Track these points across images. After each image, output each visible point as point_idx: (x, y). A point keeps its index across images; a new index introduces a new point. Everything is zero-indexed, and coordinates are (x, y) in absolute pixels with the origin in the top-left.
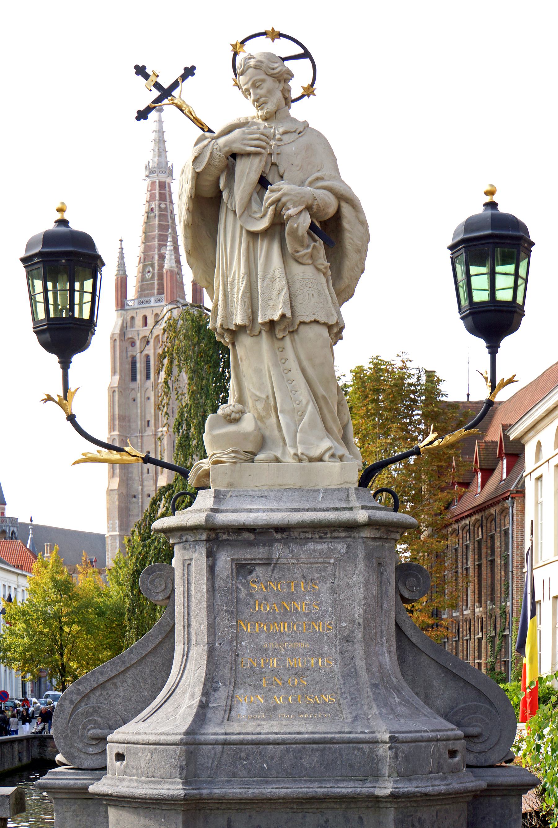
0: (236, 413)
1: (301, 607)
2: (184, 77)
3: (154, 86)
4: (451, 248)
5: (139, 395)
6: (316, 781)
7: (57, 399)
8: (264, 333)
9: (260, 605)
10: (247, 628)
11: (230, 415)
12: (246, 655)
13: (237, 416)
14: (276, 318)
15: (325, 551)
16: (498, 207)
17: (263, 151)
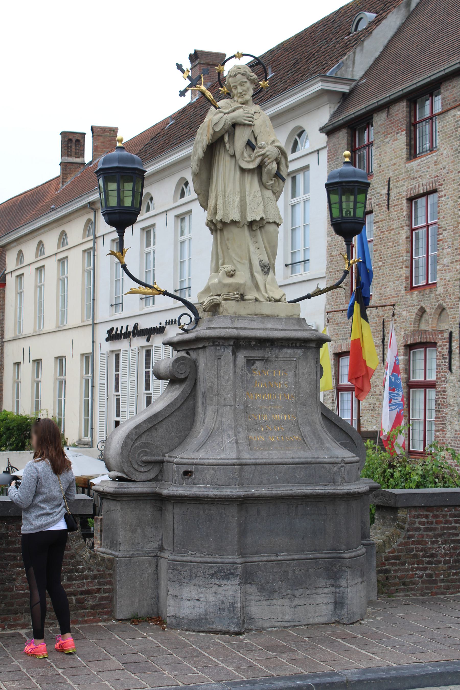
1: (279, 385)
6: (303, 486)
9: (257, 384)
10: (251, 398)
14: (258, 219)
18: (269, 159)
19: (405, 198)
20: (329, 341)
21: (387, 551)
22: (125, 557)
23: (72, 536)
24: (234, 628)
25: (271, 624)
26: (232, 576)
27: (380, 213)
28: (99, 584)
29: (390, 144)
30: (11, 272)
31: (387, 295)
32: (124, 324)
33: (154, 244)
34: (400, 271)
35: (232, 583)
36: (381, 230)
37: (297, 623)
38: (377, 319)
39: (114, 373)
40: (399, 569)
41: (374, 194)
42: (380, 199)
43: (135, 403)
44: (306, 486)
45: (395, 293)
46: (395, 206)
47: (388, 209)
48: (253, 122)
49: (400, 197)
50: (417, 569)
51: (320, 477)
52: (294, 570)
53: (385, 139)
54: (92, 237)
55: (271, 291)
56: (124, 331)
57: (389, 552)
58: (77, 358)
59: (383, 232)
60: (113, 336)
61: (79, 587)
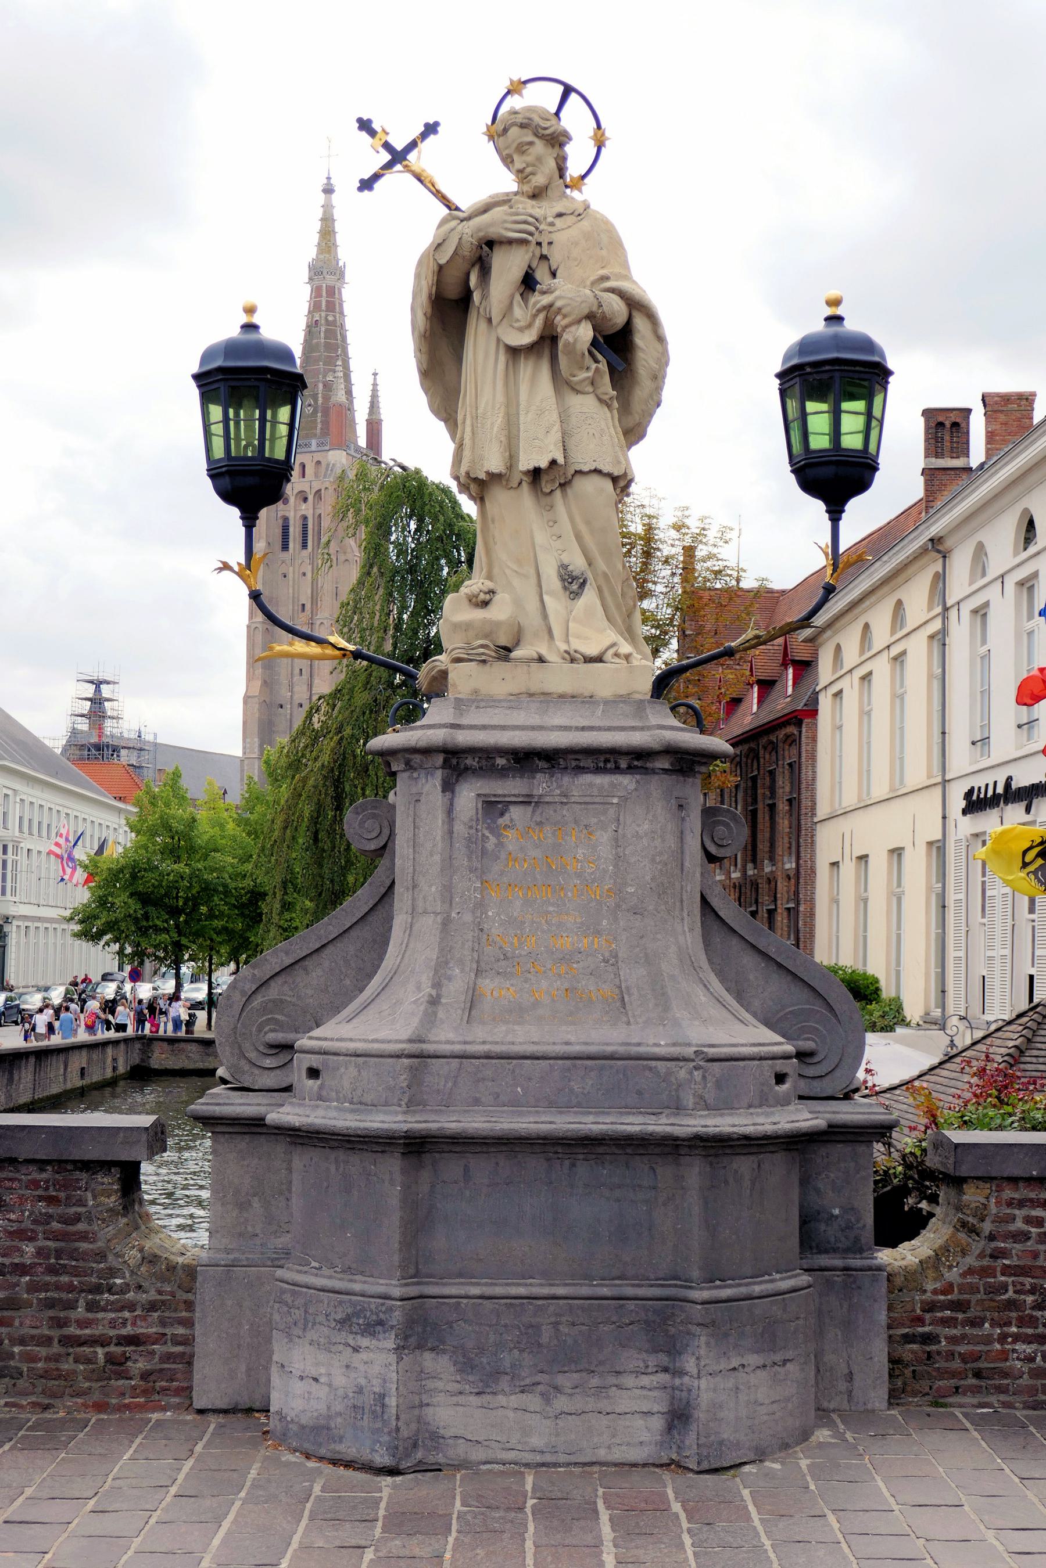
0: (486, 593)
2: (424, 136)
4: (779, 376)
5: (291, 569)
6: (590, 1113)
7: (236, 568)
8: (525, 485)
11: (477, 596)
12: (493, 930)
13: (488, 597)
15: (606, 786)
16: (261, 330)
17: (530, 238)
18: (565, 316)
21: (930, 1286)
22: (218, 1266)
23: (100, 1209)
24: (382, 1459)
25: (490, 1455)
26: (379, 1328)
28: (163, 1323)
30: (826, 687)
32: (988, 779)
35: (381, 1345)
37: (562, 1458)
39: (980, 879)
40: (964, 1336)
43: (1009, 939)
44: (596, 1113)
48: (531, 234)
50: (1017, 1338)
51: (639, 1093)
52: (556, 1324)
54: (939, 609)
55: (578, 637)
56: (990, 793)
57: (935, 1292)
58: (922, 849)
60: (975, 803)
61: (114, 1327)
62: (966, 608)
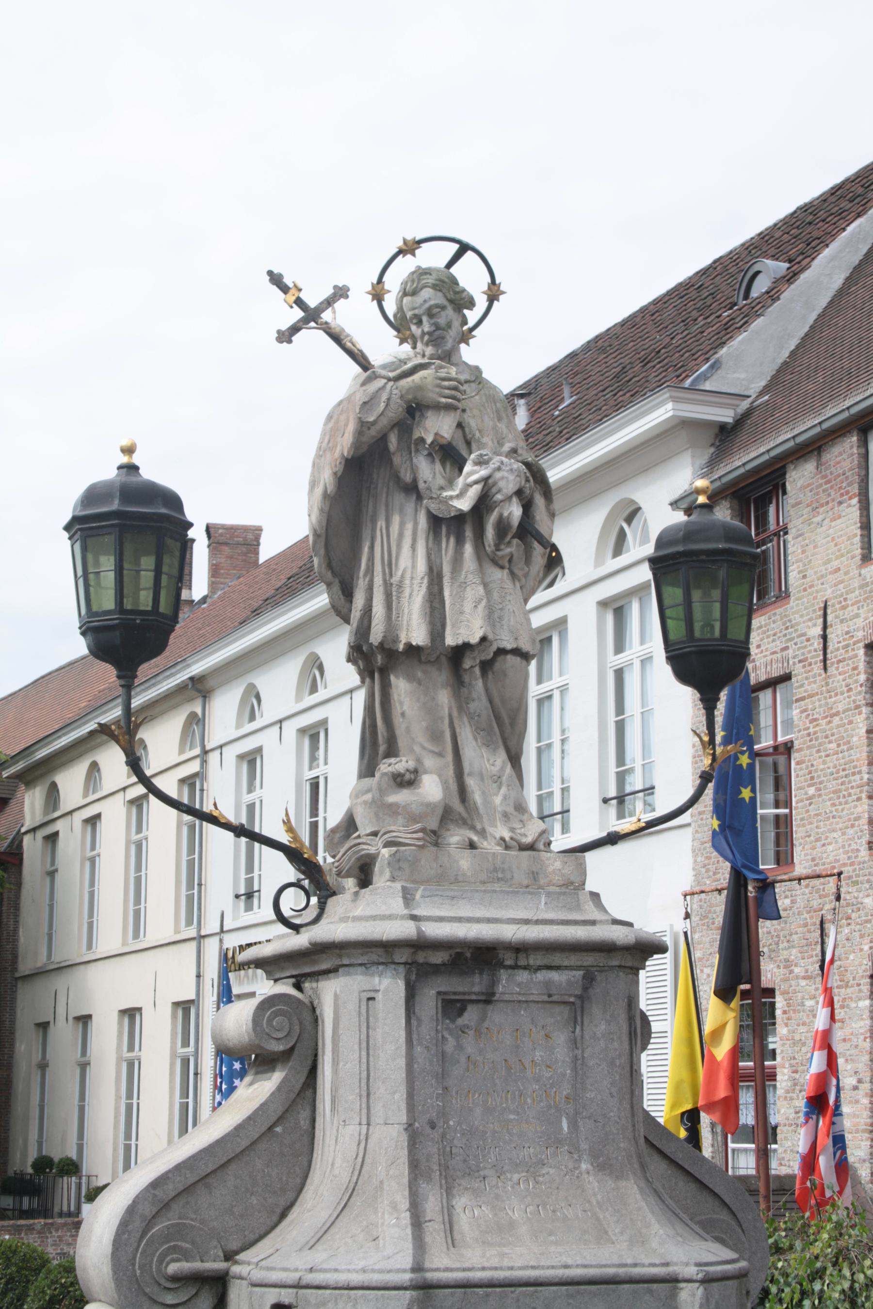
3: (295, 302)
13: (412, 776)
16: (140, 471)
19: (862, 645)
20: (661, 949)
27: (807, 678)
29: (824, 528)
31: (828, 860)
33: (326, 763)
34: (856, 806)
36: (811, 717)
38: (808, 916)
41: (793, 639)
42: (805, 647)
45: (845, 856)
46: (839, 661)
47: (825, 668)
49: (851, 642)
53: (814, 517)
54: (197, 751)
58: (167, 1010)
59: (816, 720)
62: (231, 753)
